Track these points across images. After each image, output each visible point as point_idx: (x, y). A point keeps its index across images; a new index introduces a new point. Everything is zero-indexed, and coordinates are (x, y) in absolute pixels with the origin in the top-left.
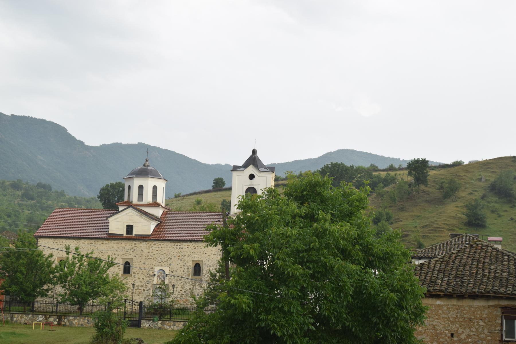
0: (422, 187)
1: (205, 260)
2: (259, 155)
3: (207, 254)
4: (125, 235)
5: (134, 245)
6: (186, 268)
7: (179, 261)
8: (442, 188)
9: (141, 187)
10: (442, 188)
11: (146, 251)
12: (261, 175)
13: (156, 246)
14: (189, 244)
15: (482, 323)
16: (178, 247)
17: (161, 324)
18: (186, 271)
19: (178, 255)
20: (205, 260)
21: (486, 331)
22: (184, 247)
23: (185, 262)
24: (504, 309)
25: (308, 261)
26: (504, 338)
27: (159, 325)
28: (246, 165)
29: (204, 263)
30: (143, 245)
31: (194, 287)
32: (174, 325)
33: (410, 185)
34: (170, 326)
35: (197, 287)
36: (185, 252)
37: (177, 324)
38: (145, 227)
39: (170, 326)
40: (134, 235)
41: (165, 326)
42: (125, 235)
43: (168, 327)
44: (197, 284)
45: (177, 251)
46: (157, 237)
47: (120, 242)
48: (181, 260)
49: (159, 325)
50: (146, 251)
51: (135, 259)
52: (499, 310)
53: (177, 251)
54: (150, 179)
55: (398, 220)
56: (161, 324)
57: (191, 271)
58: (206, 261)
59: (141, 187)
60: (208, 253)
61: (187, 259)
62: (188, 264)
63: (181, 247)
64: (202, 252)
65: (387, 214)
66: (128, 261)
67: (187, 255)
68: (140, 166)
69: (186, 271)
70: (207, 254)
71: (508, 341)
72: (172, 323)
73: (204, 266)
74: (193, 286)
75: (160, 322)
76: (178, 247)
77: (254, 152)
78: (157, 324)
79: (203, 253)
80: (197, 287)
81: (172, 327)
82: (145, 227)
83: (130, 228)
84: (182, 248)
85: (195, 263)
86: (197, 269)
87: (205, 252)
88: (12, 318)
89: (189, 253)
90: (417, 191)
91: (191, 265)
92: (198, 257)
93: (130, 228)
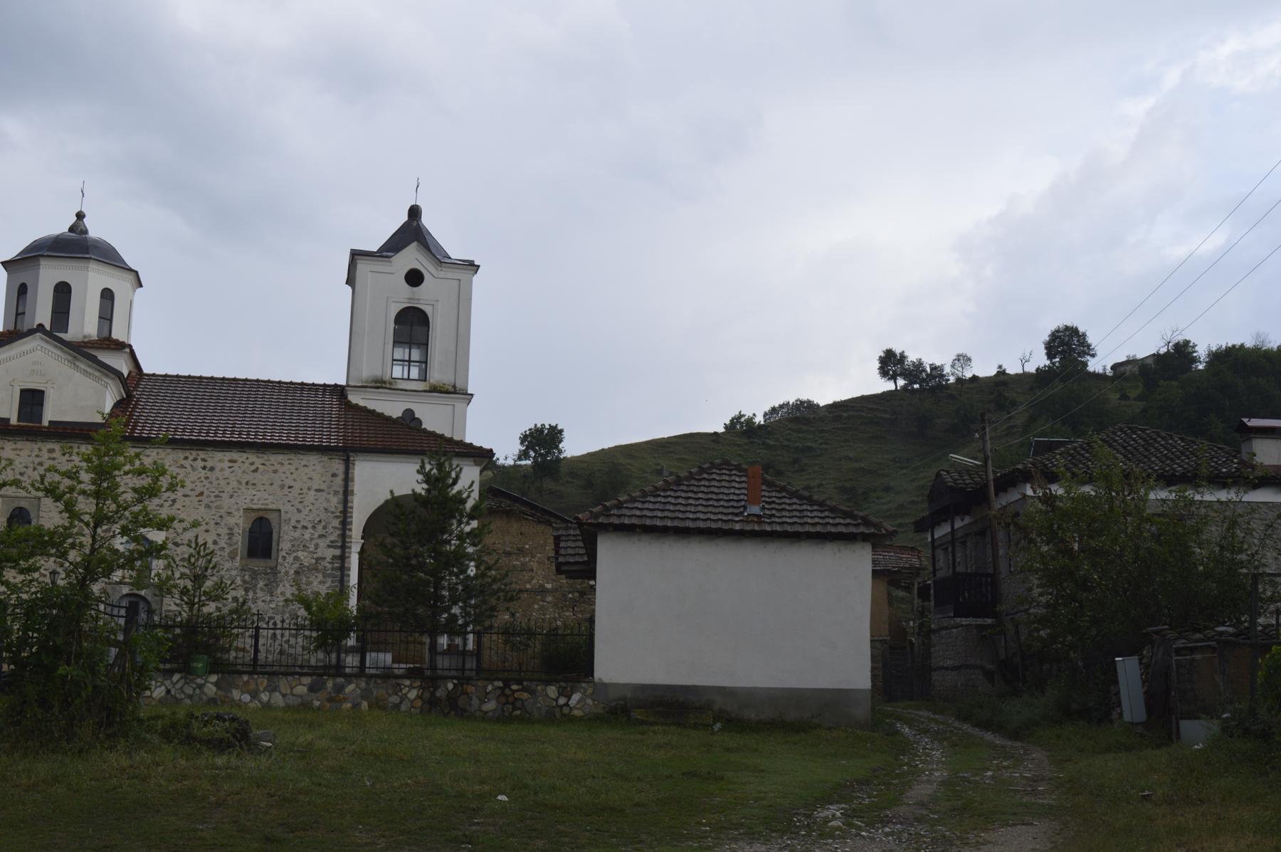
1: (288, 507)
2: (426, 220)
3: (296, 491)
4: (14, 421)
5: (45, 455)
6: (224, 531)
7: (202, 509)
12: (442, 274)
14: (234, 455)
16: (200, 464)
17: (216, 684)
18: (222, 544)
19: (199, 490)
20: (288, 507)
22: (219, 465)
23: (222, 512)
25: (700, 473)
27: (211, 690)
29: (284, 516)
31: (251, 594)
32: (272, 689)
34: (255, 695)
35: (260, 594)
36: (223, 483)
37: (283, 684)
39: (255, 695)
40: (45, 423)
41: (236, 694)
42: (14, 421)
43: (246, 698)
44: (261, 584)
45: (194, 476)
48: (208, 506)
49: (211, 690)
53: (194, 476)
54: (93, 266)
56: (216, 684)
57: (240, 541)
59: (63, 292)
60: (297, 485)
61: (226, 502)
62: (232, 521)
63: (209, 464)
64: (277, 483)
66: (23, 504)
67: (229, 489)
68: (60, 226)
69: (222, 544)
70: (296, 491)
72: (264, 681)
73: (285, 528)
74: (246, 590)
75: (214, 678)
76: (201, 464)
78: (200, 687)
79: (282, 487)
80: (260, 594)
81: (264, 697)
83: (32, 400)
84: (212, 469)
85: (254, 515)
86: (261, 538)
87: (289, 482)
89: (235, 484)
91: (240, 523)
92: (262, 498)
93: (32, 400)
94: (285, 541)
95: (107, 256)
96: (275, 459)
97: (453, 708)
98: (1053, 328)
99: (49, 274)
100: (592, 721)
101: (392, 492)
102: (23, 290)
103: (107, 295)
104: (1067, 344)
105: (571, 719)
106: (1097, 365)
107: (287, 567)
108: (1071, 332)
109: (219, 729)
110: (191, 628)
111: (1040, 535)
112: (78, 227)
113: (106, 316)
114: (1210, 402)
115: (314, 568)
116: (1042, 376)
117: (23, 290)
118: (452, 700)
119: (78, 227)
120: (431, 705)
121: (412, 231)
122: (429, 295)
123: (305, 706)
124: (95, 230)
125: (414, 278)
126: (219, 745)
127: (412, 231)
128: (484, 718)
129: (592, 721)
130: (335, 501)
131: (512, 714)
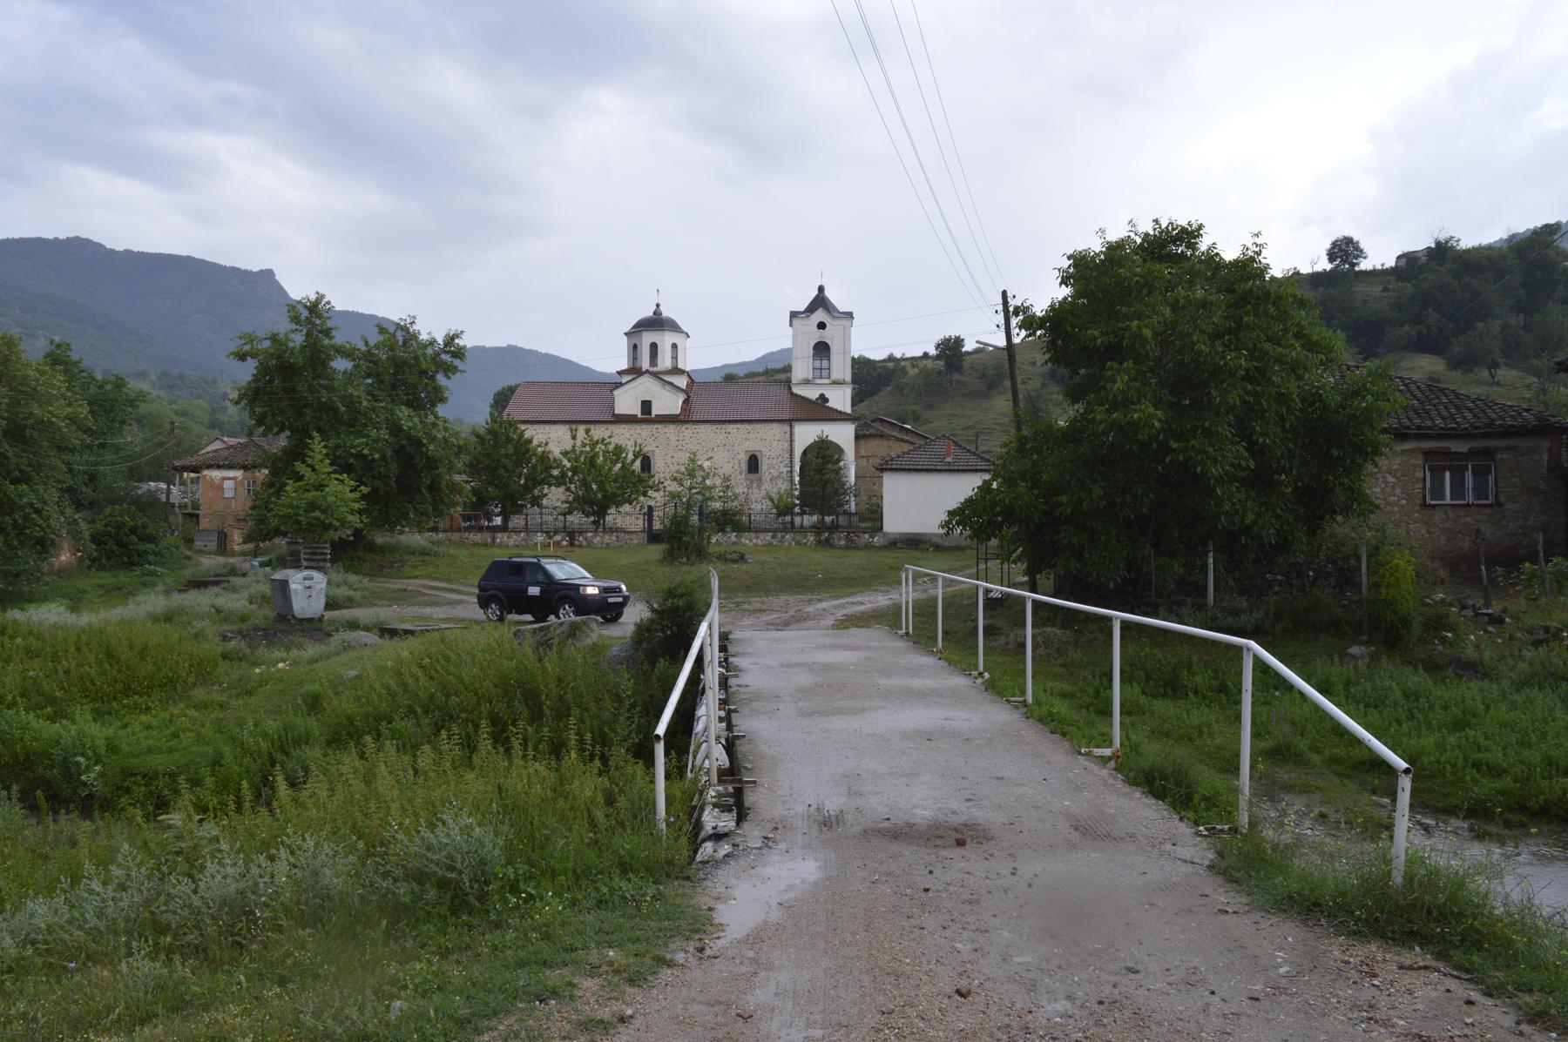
0: (956, 376)
2: (827, 293)
8: (984, 376)
9: (654, 347)
10: (984, 376)
11: (673, 438)
13: (688, 431)
15: (1391, 479)
21: (1398, 491)
24: (1428, 454)
26: (1428, 501)
28: (811, 309)
30: (670, 430)
33: (940, 372)
38: (668, 403)
46: (680, 420)
47: (634, 426)
50: (673, 438)
51: (657, 452)
52: (1421, 456)
55: (928, 421)
57: (744, 466)
58: (765, 451)
59: (654, 347)
61: (737, 448)
65: (914, 412)
68: (648, 312)
71: (1434, 506)
77: (821, 289)
82: (668, 403)
83: (646, 406)
86: (753, 464)
88: (493, 539)
90: (950, 382)
91: (744, 458)
92: (753, 446)
93: (646, 406)
94: (764, 465)
95: (672, 326)
96: (758, 426)
97: (828, 544)
98: (1334, 238)
99: (647, 338)
100: (885, 547)
101: (1156, 221)
102: (635, 346)
103: (674, 346)
104: (1344, 250)
105: (873, 547)
106: (1365, 265)
107: (766, 477)
108: (1348, 241)
109: (734, 556)
110: (725, 513)
111: (1035, 463)
112: (657, 313)
113: (675, 357)
114: (1535, 260)
115: (778, 477)
116: (1317, 279)
117: (635, 346)
118: (827, 540)
119: (657, 313)
120: (819, 542)
121: (820, 301)
122: (831, 335)
123: (770, 544)
124: (666, 312)
125: (822, 326)
126: (735, 561)
127: (820, 301)
128: (840, 548)
129: (885, 547)
130: (787, 445)
131: (851, 546)
